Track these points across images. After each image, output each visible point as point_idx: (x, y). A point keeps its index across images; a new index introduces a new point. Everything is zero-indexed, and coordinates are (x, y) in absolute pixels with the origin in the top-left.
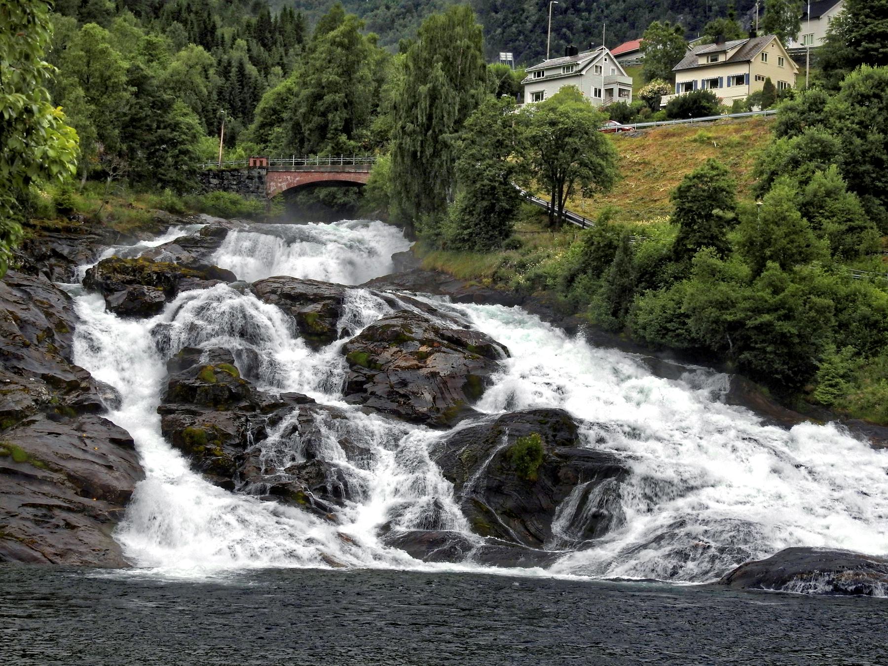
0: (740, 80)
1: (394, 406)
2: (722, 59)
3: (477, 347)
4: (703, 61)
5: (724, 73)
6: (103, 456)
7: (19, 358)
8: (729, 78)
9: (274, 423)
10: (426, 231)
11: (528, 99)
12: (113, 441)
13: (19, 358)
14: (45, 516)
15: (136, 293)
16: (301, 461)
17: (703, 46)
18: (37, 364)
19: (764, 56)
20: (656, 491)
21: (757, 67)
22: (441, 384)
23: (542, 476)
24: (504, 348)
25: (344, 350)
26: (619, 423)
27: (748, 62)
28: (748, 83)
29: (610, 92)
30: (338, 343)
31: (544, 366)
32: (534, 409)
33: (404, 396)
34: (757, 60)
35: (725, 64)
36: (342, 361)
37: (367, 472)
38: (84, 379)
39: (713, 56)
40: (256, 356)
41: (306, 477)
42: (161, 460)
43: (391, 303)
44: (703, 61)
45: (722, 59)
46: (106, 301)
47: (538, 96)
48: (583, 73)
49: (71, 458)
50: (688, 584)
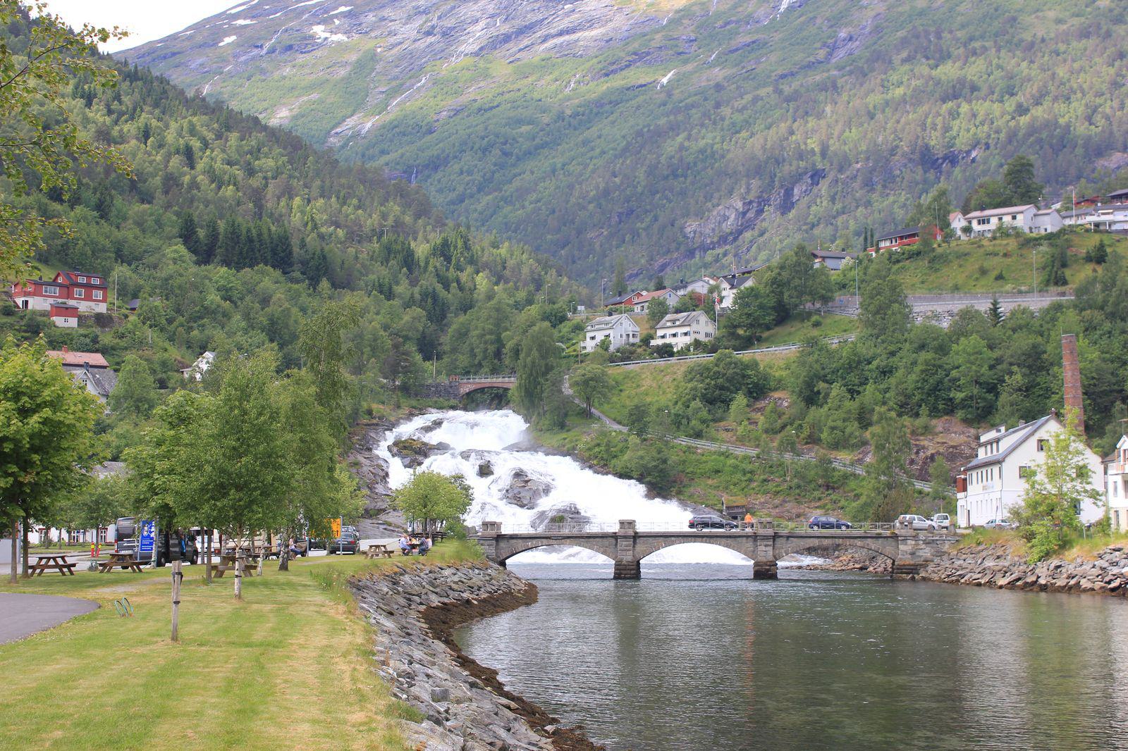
29: (628, 335)
35: (679, 326)
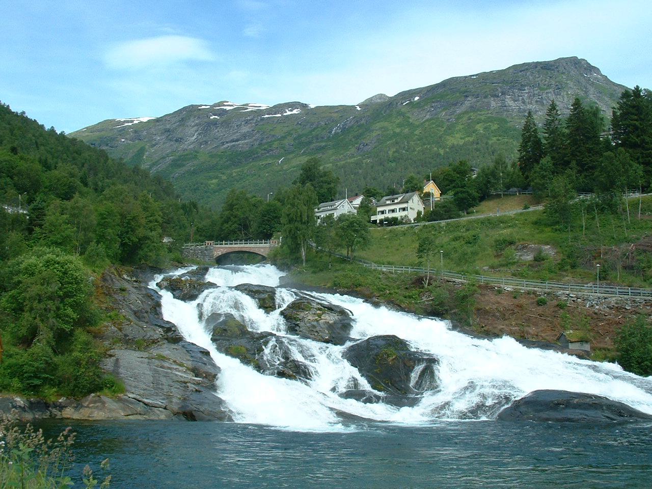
2: (396, 201)
5: (397, 207)
8: (399, 209)
9: (266, 343)
10: (6, 372)
12: (201, 352)
15: (186, 291)
16: (283, 360)
17: (256, 251)
22: (330, 327)
24: (351, 312)
25: (282, 313)
27: (407, 202)
28: (407, 210)
30: (278, 311)
34: (410, 202)
36: (282, 320)
37: (314, 363)
38: (173, 327)
40: (243, 316)
41: (289, 367)
42: (220, 359)
43: (296, 294)
44: (388, 202)
46: (173, 294)
48: (338, 208)
50: (139, 417)
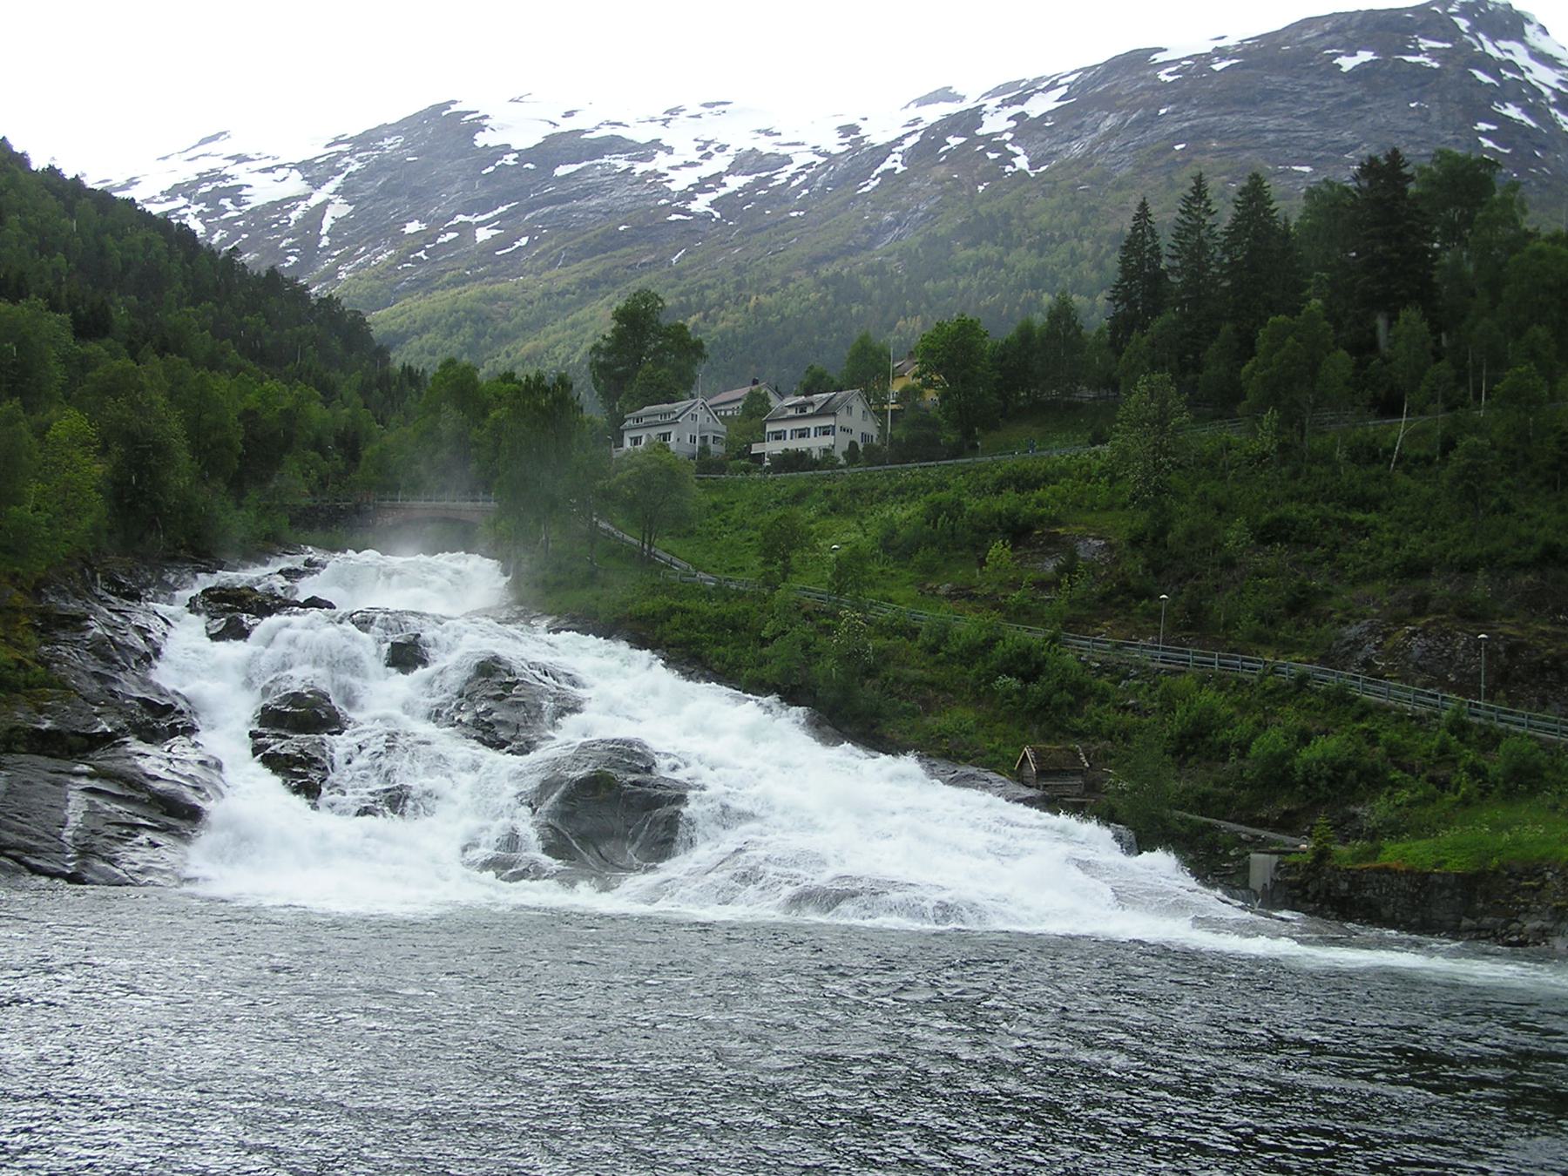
0: (826, 431)
1: (480, 733)
3: (341, 512)
4: (792, 412)
5: (811, 424)
6: (191, 777)
7: (115, 681)
11: (627, 444)
13: (115, 681)
14: (128, 834)
15: (232, 613)
18: (133, 688)
19: (849, 408)
20: (727, 816)
21: (842, 419)
23: (618, 811)
26: (278, 665)
31: (628, 697)
32: (942, 766)
33: (489, 724)
34: (842, 414)
39: (801, 407)
45: (810, 410)
47: (636, 441)
49: (157, 778)
